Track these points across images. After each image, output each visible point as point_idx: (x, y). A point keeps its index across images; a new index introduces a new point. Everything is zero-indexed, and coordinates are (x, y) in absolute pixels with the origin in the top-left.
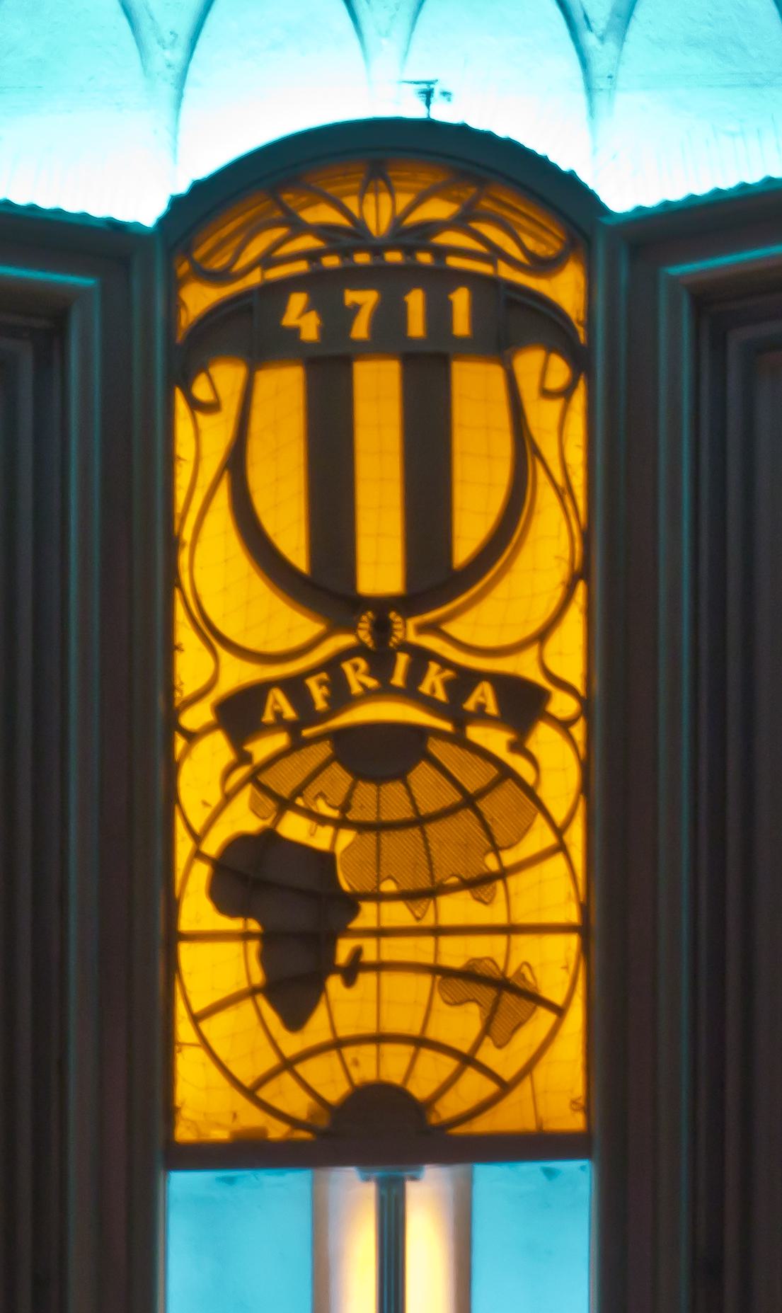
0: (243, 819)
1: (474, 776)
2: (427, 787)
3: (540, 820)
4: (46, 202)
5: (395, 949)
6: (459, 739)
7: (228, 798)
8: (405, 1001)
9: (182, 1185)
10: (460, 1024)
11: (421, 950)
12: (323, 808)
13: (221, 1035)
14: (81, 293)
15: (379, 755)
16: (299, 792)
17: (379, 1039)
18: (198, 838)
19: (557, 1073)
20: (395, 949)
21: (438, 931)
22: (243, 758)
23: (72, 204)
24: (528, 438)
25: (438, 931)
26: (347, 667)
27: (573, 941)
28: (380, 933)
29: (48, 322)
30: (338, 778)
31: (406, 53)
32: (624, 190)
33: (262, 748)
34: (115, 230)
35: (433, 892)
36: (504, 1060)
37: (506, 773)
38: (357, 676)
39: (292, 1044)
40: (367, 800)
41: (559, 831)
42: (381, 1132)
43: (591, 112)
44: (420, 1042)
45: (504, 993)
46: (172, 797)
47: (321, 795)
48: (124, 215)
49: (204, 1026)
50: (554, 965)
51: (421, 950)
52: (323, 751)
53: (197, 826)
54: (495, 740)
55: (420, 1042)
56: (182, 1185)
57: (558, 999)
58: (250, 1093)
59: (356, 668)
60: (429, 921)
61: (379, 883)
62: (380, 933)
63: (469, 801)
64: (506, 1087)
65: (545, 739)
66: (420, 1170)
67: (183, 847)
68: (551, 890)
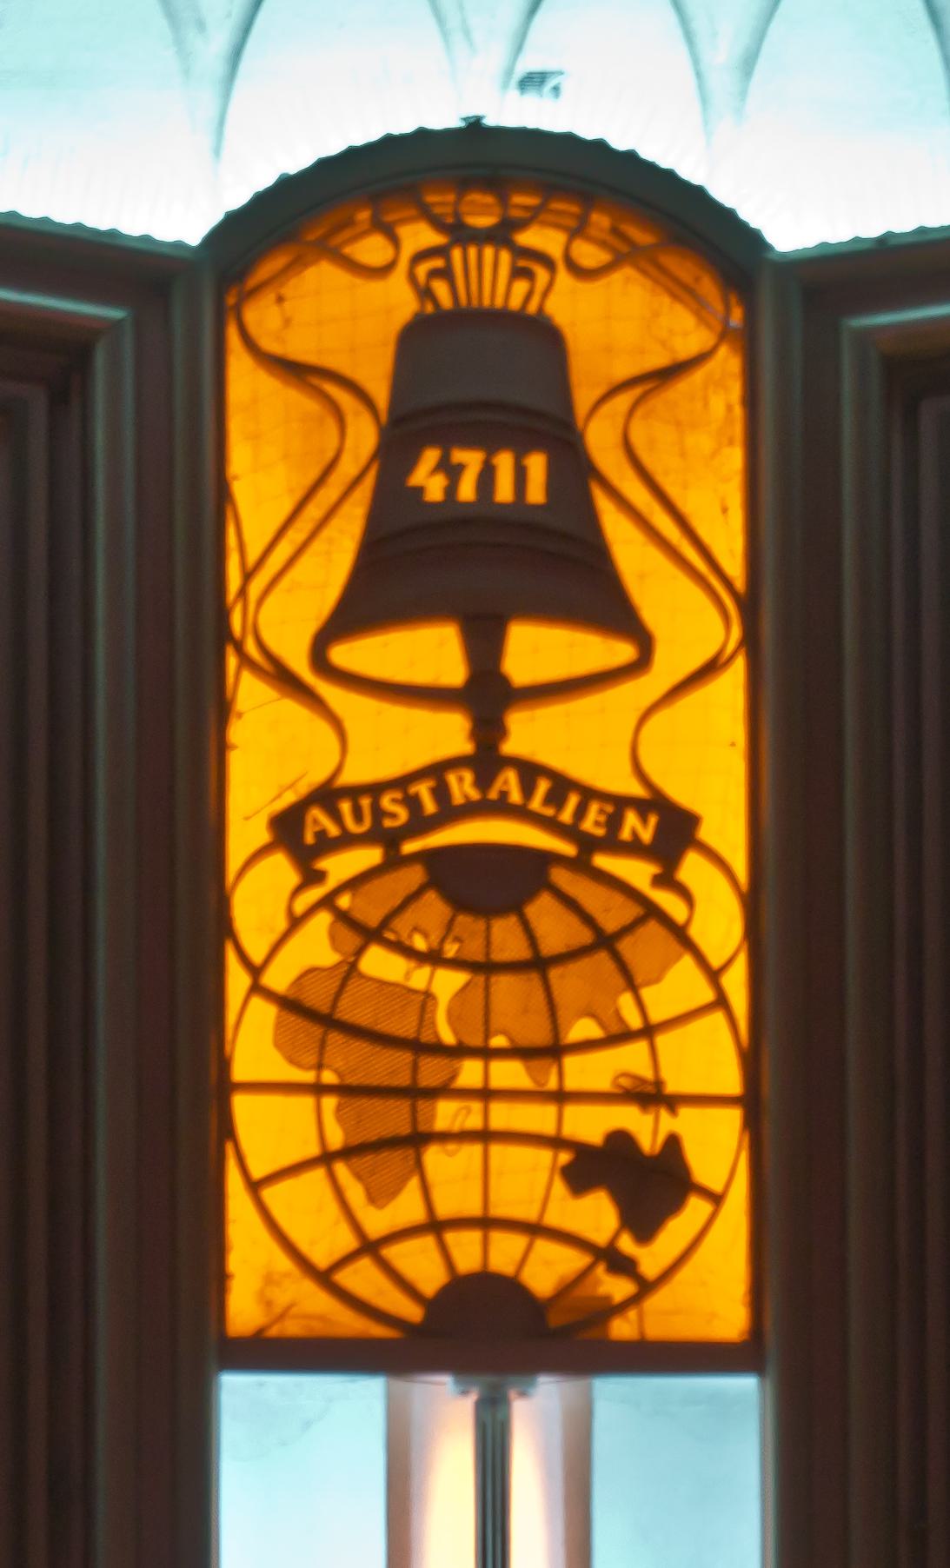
0: (315, 946)
1: (612, 913)
2: (552, 925)
3: (687, 961)
4: (65, 215)
5: (503, 1116)
6: (581, 865)
7: (295, 922)
8: (524, 1182)
9: (238, 1394)
10: (596, 1215)
11: (539, 1118)
12: (420, 943)
13: (285, 1200)
14: (117, 324)
15: (487, 884)
16: (386, 922)
17: (486, 1223)
18: (255, 971)
19: (709, 1270)
20: (503, 1116)
21: (561, 1097)
22: (311, 877)
23: (99, 218)
24: (687, 483)
25: (561, 1097)
26: (452, 778)
27: (733, 1117)
28: (486, 1094)
29: (64, 358)
30: (433, 908)
31: (217, 151)
32: (799, 208)
33: (341, 866)
34: (754, 239)
35: (555, 1051)
36: (651, 1259)
37: (653, 912)
38: (462, 786)
39: (377, 1222)
40: (470, 935)
41: (714, 976)
42: (487, 1333)
43: (706, 122)
44: (535, 1229)
45: (647, 1184)
46: (225, 928)
47: (416, 929)
48: (166, 232)
49: (269, 1194)
50: (715, 1146)
51: (539, 1118)
52: (414, 876)
53: (257, 956)
54: (638, 873)
55: (535, 1229)
56: (238, 1394)
57: (716, 1186)
58: (324, 1278)
59: (461, 780)
60: (552, 1084)
61: (487, 1036)
62: (486, 1094)
63: (605, 942)
64: (646, 1287)
65: (693, 868)
66: (532, 1384)
67: (237, 981)
68: (707, 1058)
